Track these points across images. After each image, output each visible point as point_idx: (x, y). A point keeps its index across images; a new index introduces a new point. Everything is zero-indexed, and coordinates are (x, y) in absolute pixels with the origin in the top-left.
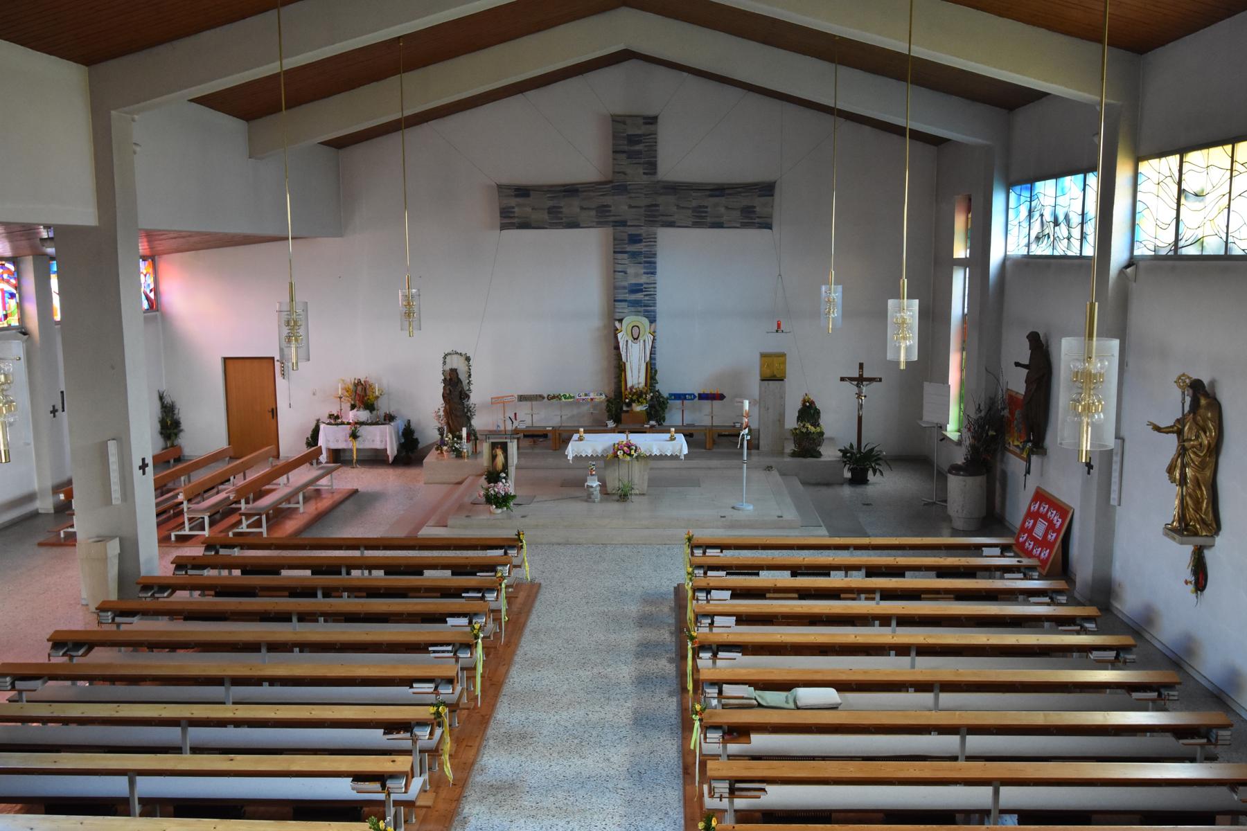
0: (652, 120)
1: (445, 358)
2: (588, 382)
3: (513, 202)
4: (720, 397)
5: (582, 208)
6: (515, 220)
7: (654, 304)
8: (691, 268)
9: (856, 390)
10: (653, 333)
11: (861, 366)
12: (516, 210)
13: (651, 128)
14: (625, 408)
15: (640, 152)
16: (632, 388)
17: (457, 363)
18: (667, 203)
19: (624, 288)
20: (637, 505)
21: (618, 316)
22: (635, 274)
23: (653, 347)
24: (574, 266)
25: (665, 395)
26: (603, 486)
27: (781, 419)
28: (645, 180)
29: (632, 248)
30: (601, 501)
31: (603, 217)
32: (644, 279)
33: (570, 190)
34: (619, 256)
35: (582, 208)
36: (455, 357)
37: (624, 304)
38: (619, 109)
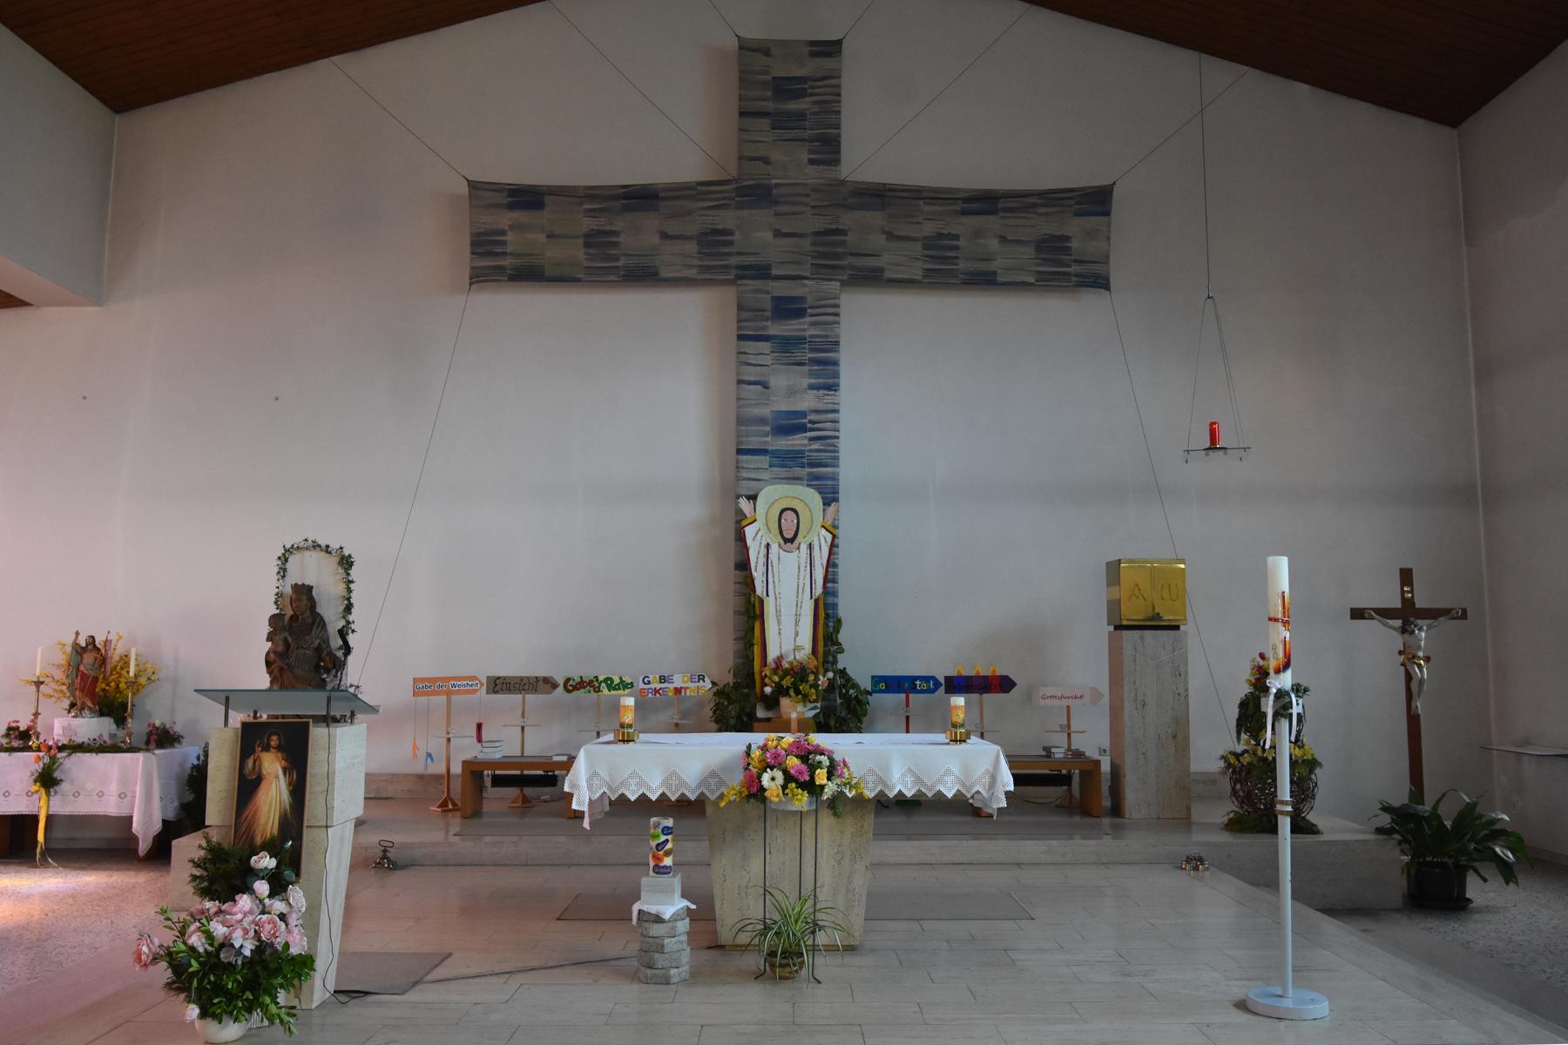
0: (830, 49)
1: (284, 559)
2: (675, 640)
3: (505, 219)
4: (1004, 684)
5: (665, 236)
6: (507, 262)
7: (834, 463)
8: (925, 391)
9: (1398, 641)
10: (833, 529)
11: (1406, 576)
12: (510, 237)
13: (828, 63)
14: (761, 713)
15: (801, 116)
16: (780, 659)
17: (317, 573)
18: (864, 228)
19: (762, 421)
20: (826, 995)
21: (746, 486)
22: (790, 389)
23: (831, 564)
24: (641, 386)
25: (866, 684)
26: (702, 915)
27: (1178, 737)
28: (813, 176)
29: (783, 324)
30: (696, 976)
31: (715, 260)
32: (808, 402)
33: (641, 198)
34: (751, 346)
35: (665, 236)
36: (312, 557)
37: (763, 461)
38: (755, 31)
